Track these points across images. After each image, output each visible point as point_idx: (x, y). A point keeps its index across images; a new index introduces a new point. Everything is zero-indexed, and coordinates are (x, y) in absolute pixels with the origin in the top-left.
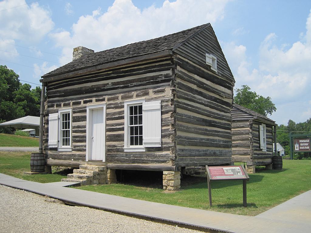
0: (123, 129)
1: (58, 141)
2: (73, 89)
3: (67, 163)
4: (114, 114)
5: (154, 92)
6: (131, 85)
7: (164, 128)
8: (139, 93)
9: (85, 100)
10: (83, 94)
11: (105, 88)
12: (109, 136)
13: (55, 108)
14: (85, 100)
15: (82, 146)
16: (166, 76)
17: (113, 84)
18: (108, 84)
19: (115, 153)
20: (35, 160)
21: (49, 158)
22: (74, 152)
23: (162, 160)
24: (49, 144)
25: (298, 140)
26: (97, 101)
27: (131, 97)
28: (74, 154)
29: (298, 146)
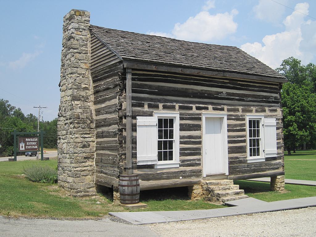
0: (244, 141)
3: (171, 182)
4: (236, 125)
5: (269, 110)
6: (246, 99)
8: (258, 109)
9: (198, 105)
10: (190, 97)
11: (219, 96)
13: (146, 108)
14: (198, 105)
15: (195, 159)
16: (275, 98)
17: (228, 94)
18: (222, 92)
19: (238, 165)
22: (182, 168)
24: (138, 159)
25: (24, 138)
26: (214, 109)
27: (251, 111)
28: (183, 170)
29: (24, 145)
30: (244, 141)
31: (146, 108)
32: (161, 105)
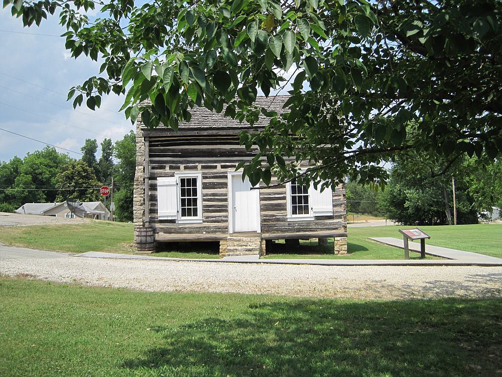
0: (284, 198)
1: (178, 212)
2: (200, 149)
7: (334, 198)
10: (217, 157)
12: (265, 205)
13: (167, 170)
19: (275, 223)
20: (149, 236)
21: (158, 233)
22: (206, 224)
23: (334, 227)
26: (186, 168)
30: (284, 198)
31: (167, 170)
32: (182, 166)
